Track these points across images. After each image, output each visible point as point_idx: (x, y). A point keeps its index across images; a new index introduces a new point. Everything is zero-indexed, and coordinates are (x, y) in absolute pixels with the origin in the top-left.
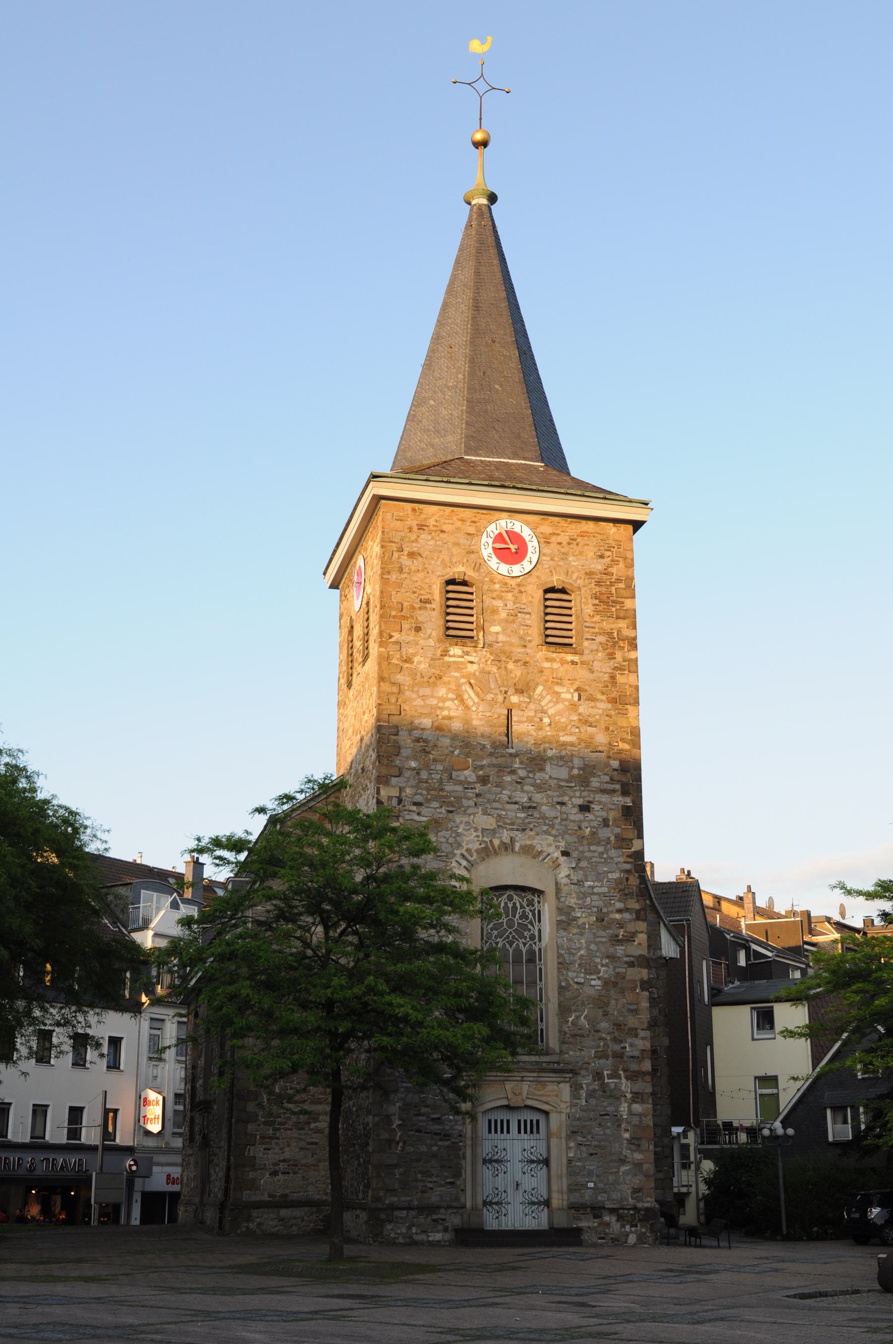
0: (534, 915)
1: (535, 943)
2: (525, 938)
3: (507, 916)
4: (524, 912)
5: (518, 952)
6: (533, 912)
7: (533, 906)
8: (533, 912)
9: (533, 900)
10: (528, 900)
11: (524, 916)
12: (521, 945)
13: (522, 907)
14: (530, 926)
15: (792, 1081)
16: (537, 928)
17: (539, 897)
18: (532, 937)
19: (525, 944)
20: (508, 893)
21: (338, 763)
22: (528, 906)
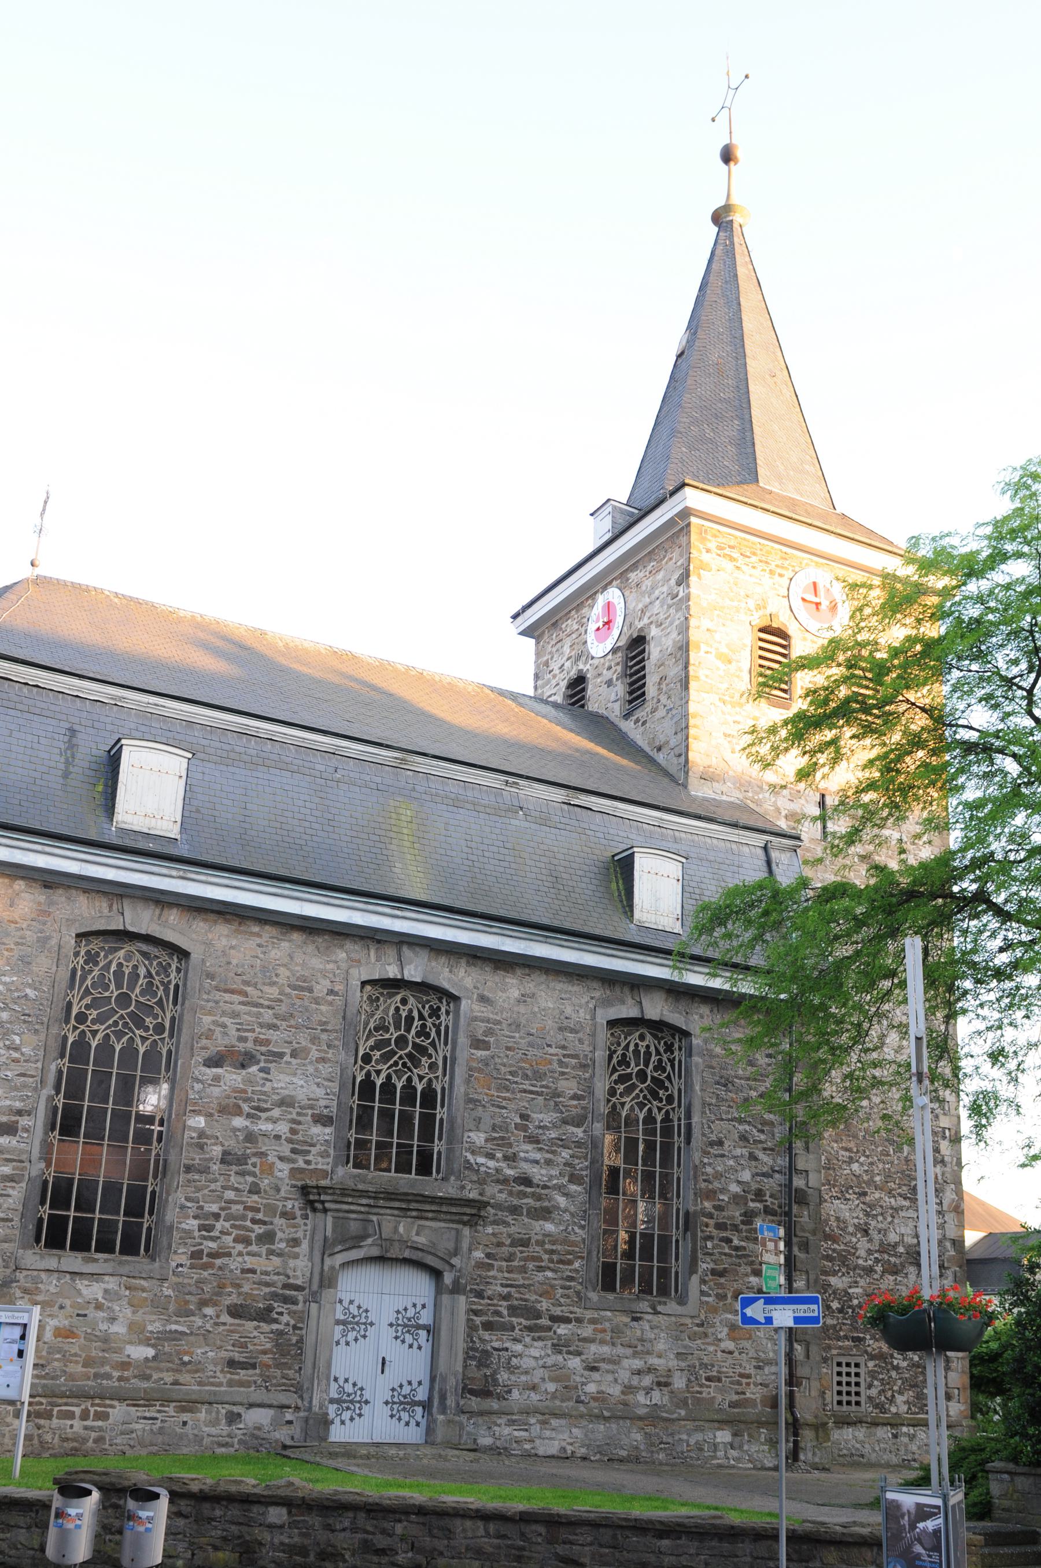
0: (438, 1033)
1: (437, 1078)
2: (147, 1029)
3: (119, 986)
4: (660, 1061)
5: (409, 1086)
6: (438, 1027)
7: (438, 1017)
8: (438, 1027)
9: (439, 1008)
10: (665, 1043)
11: (423, 1032)
12: (655, 1110)
13: (421, 1017)
14: (431, 1051)
15: (818, 798)
16: (169, 1015)
17: (180, 961)
18: (670, 1099)
19: (660, 1109)
20: (128, 947)
21: (955, 1025)
22: (665, 1052)
